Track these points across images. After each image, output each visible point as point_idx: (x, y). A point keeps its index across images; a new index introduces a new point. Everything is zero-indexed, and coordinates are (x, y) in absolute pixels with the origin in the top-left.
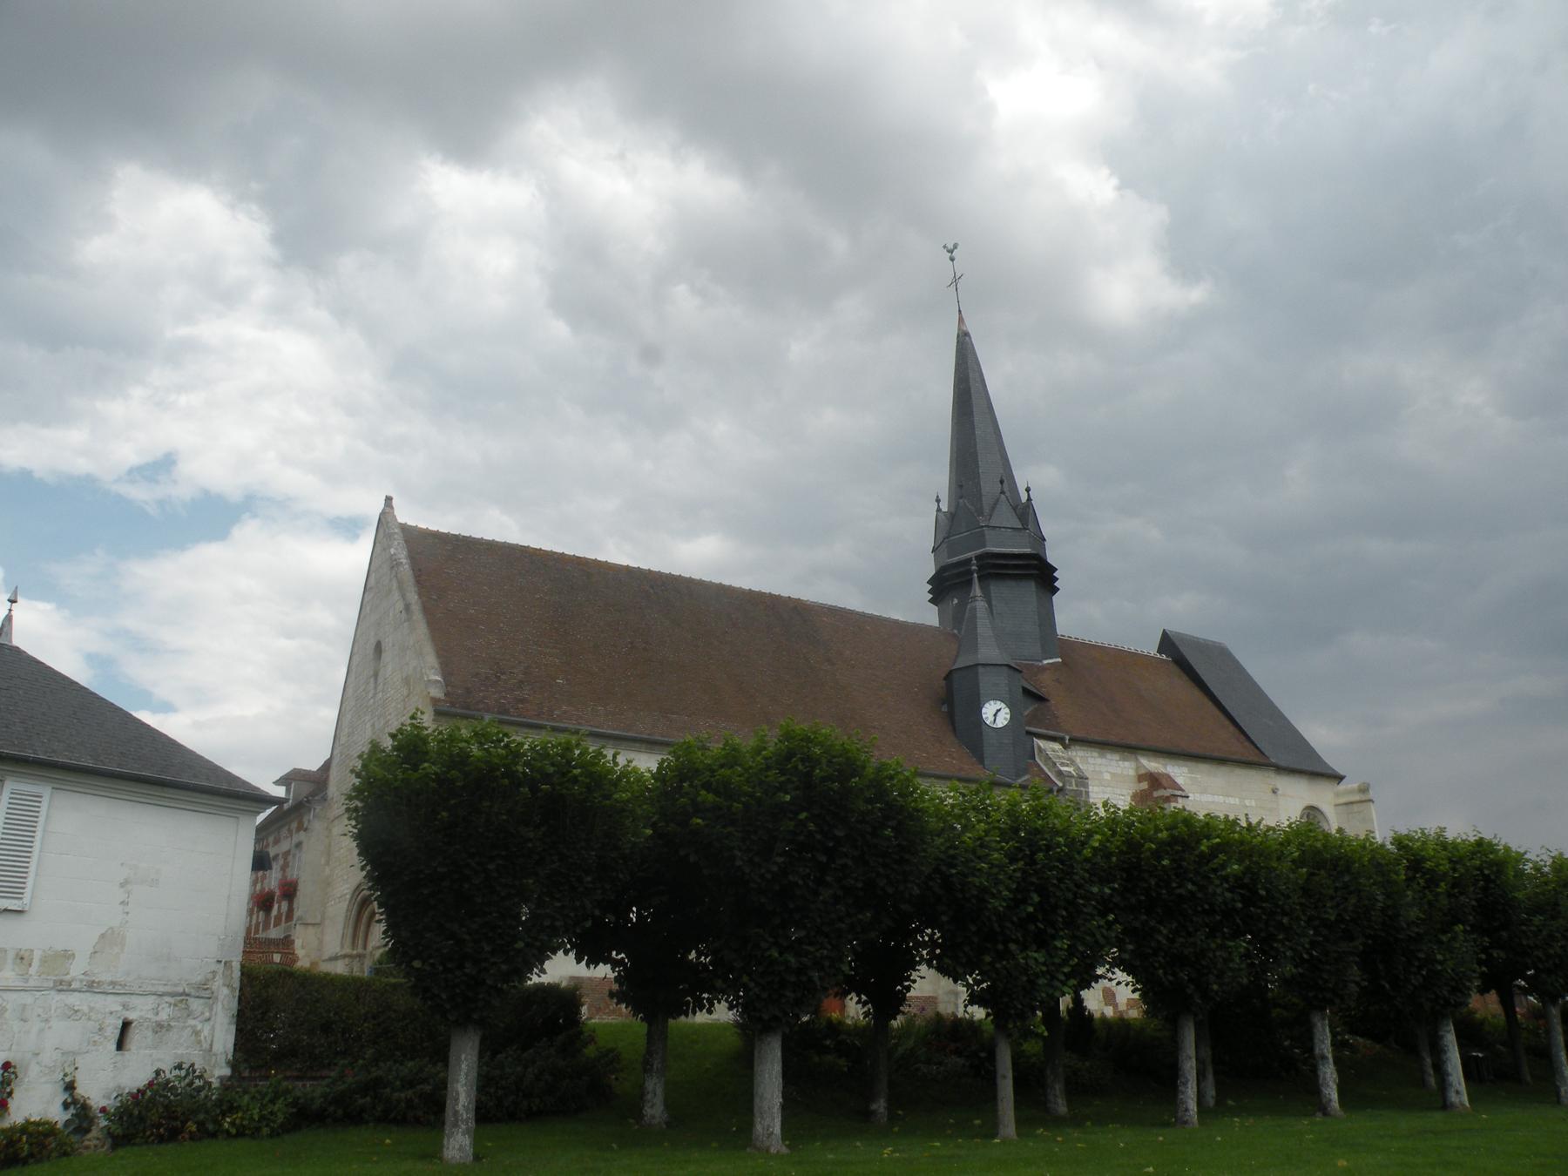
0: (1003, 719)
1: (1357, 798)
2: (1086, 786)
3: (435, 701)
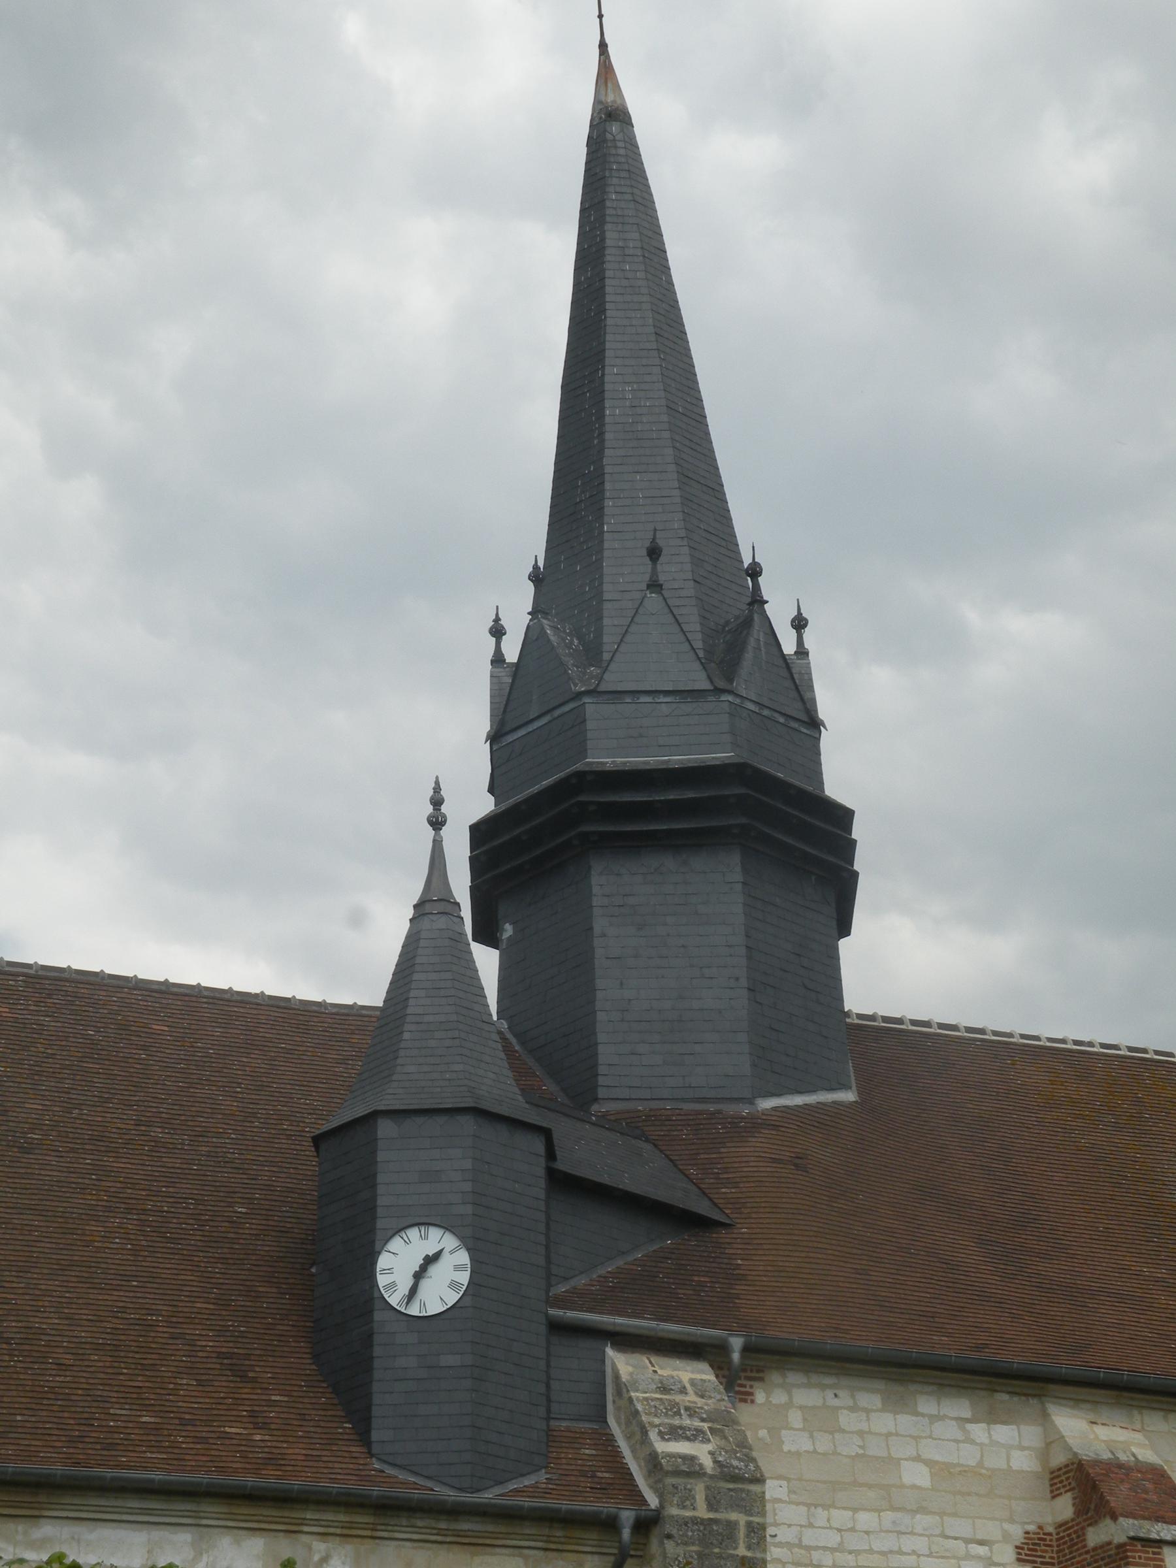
0: (441, 1292)
2: (755, 1504)
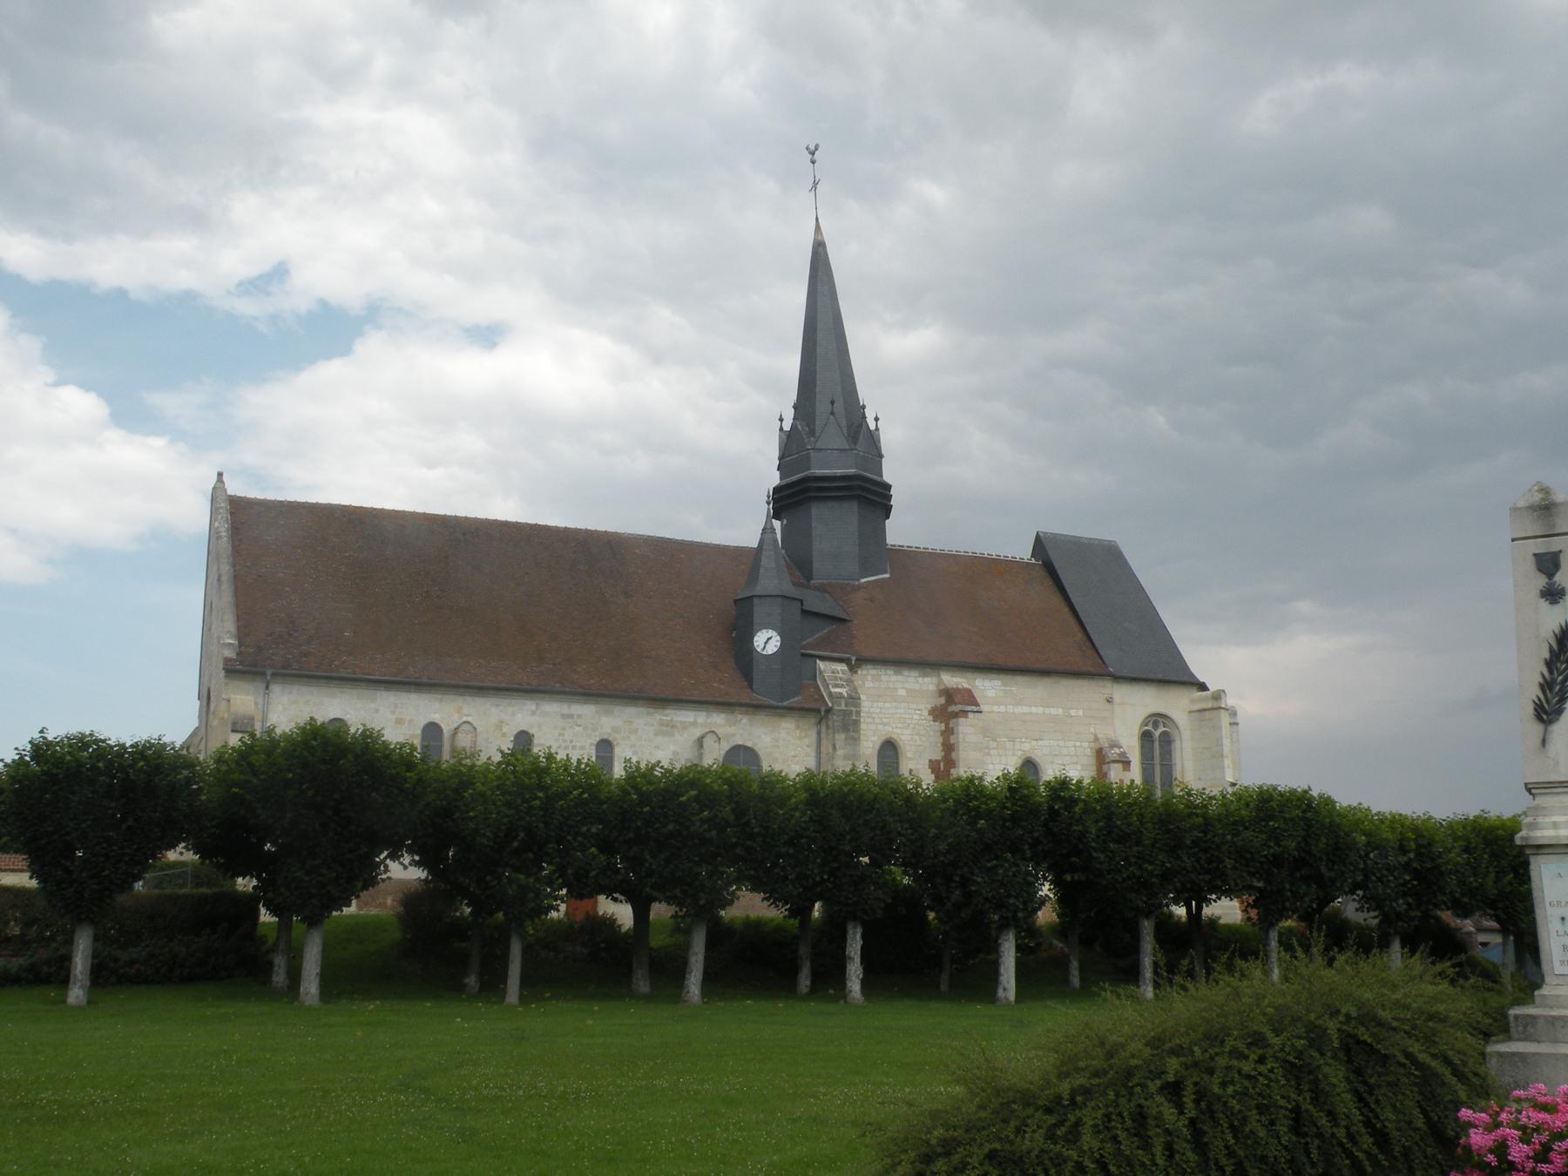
0: (772, 648)
1: (1210, 705)
2: (858, 705)
3: (226, 660)
